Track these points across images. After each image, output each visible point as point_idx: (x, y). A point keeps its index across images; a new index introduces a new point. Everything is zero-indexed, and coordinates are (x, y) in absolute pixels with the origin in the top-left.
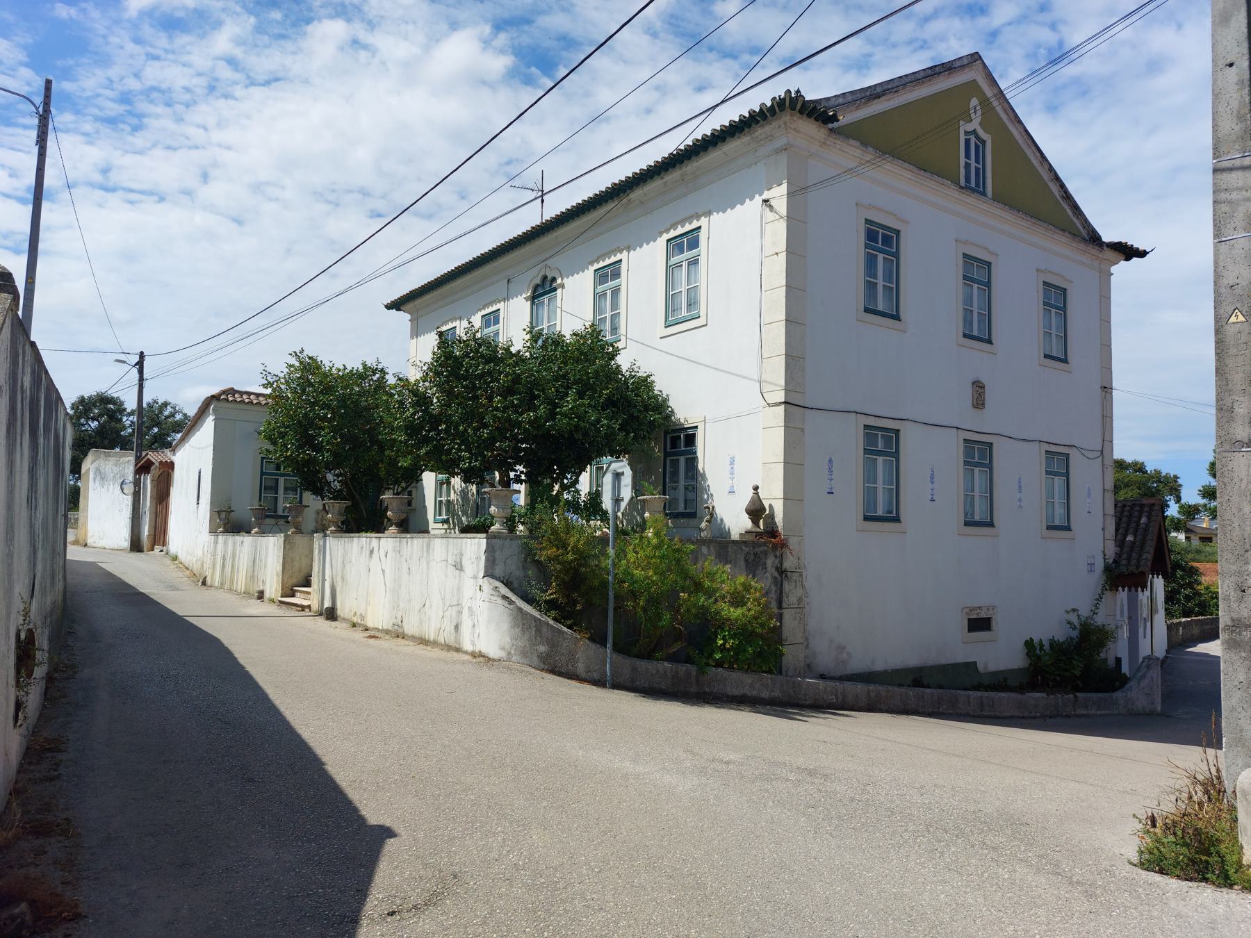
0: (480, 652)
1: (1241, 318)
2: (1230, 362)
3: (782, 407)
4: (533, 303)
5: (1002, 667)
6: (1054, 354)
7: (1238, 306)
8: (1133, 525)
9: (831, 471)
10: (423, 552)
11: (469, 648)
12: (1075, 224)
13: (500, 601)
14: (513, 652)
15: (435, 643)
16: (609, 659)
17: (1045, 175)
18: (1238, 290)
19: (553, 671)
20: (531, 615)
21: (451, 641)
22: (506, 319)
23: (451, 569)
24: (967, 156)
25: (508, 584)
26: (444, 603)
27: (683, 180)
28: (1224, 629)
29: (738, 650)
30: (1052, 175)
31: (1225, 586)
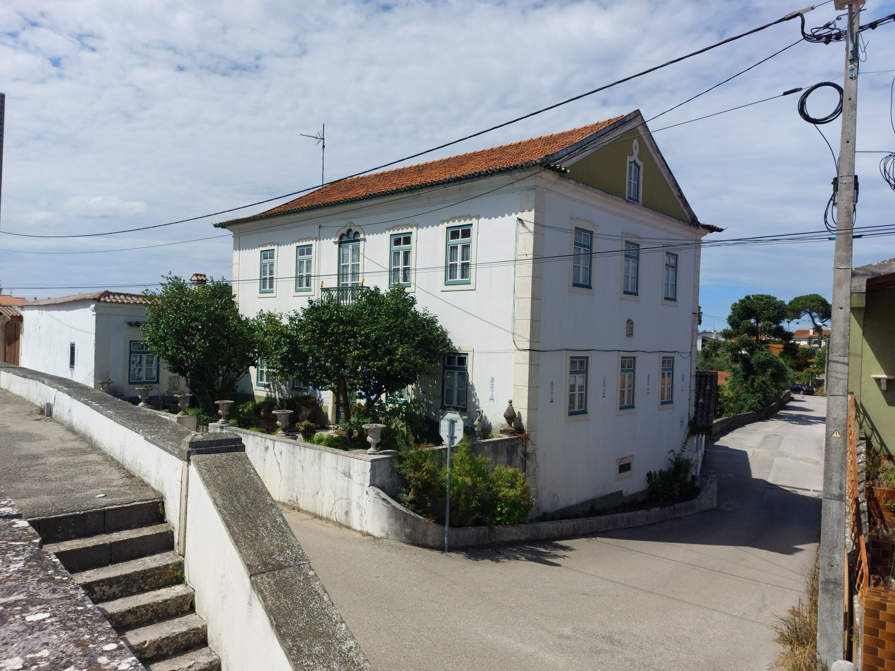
0: (367, 532)
1: (838, 436)
2: (832, 455)
3: (528, 352)
4: (340, 246)
5: (635, 491)
6: (669, 296)
7: (837, 429)
8: (702, 391)
9: (552, 388)
10: (315, 458)
11: (359, 528)
12: (684, 213)
13: (381, 502)
14: (390, 533)
15: (328, 520)
16: (446, 533)
17: (670, 184)
18: (838, 421)
19: (414, 544)
20: (401, 511)
21: (342, 520)
22: (317, 251)
23: (340, 475)
24: (630, 178)
25: (382, 488)
26: (335, 496)
27: (460, 191)
28: (821, 583)
29: (510, 513)
30: (674, 184)
31: (823, 563)
